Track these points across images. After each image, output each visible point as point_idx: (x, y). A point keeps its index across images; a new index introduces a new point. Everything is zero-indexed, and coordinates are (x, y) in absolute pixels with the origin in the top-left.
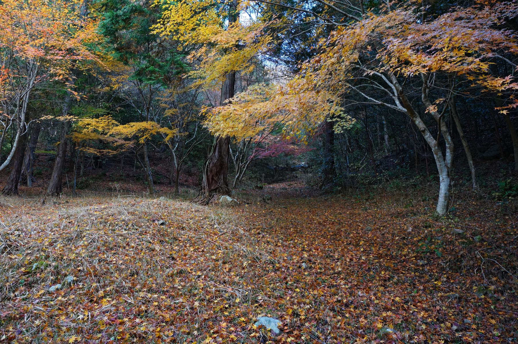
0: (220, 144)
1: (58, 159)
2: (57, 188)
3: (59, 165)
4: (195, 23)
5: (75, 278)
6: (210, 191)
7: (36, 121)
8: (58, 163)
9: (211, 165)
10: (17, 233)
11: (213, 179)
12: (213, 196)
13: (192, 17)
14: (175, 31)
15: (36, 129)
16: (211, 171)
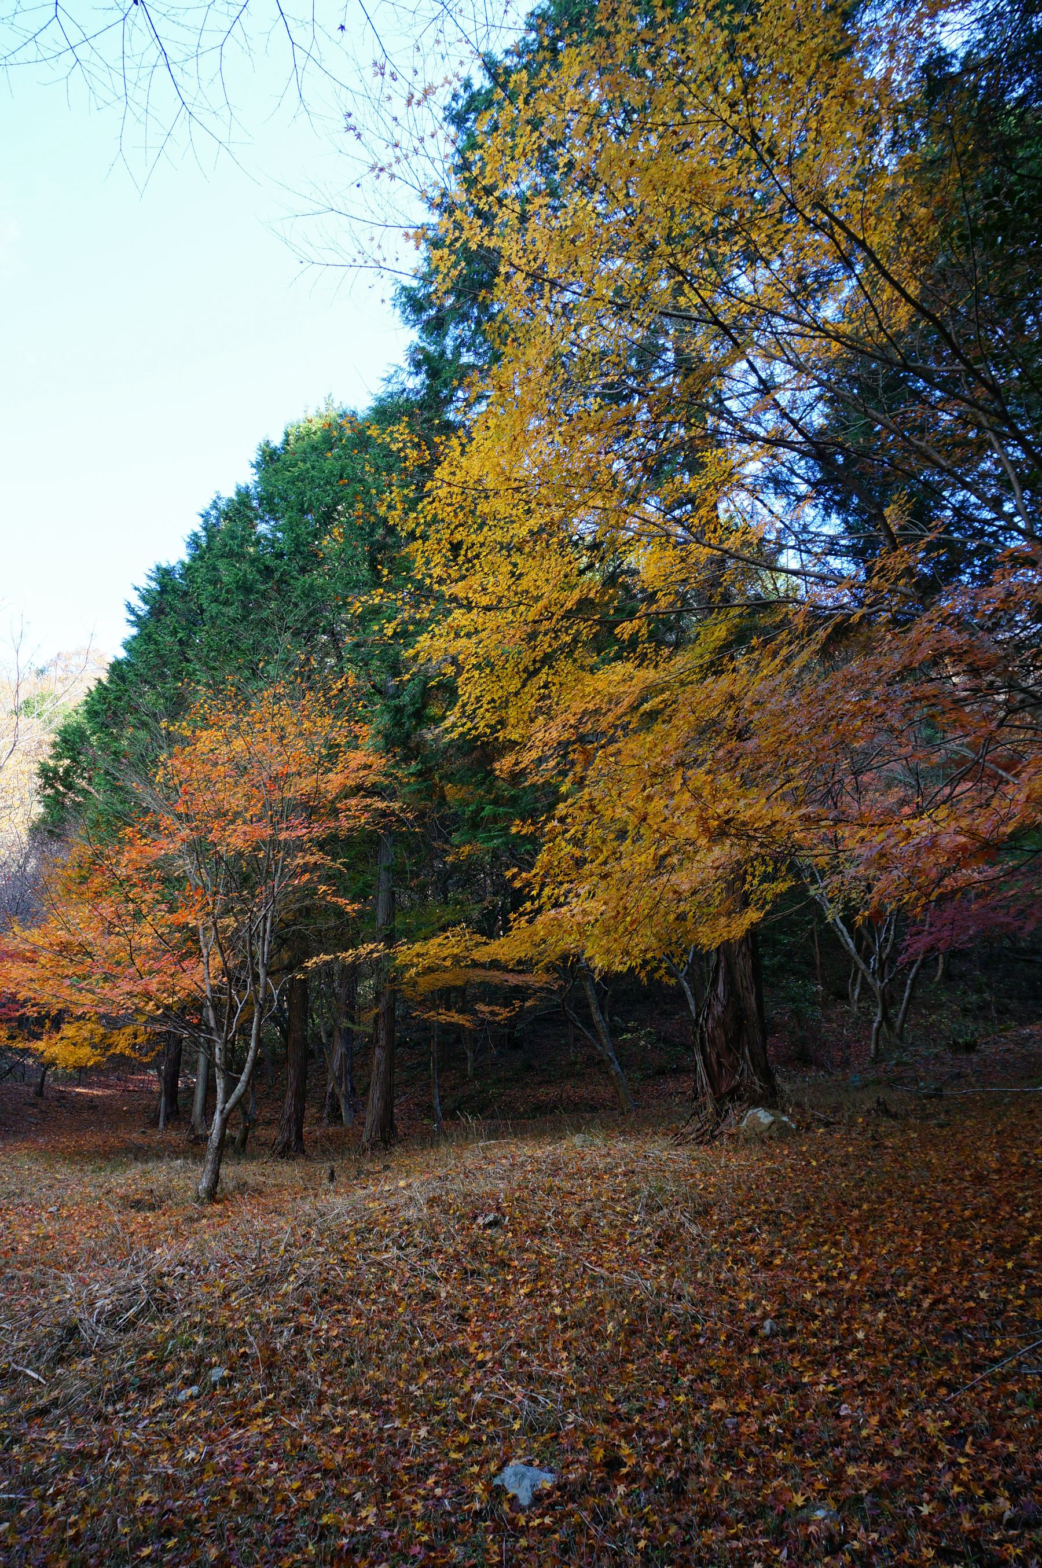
0: (727, 959)
1: (378, 1051)
2: (383, 1130)
3: (382, 1068)
4: (537, 697)
5: (226, 1373)
6: (719, 1100)
7: (294, 978)
8: (379, 1064)
9: (710, 1024)
10: (180, 1270)
11: (720, 1065)
12: (727, 1111)
13: (524, 686)
14: (499, 722)
15: (299, 993)
16: (712, 1042)
